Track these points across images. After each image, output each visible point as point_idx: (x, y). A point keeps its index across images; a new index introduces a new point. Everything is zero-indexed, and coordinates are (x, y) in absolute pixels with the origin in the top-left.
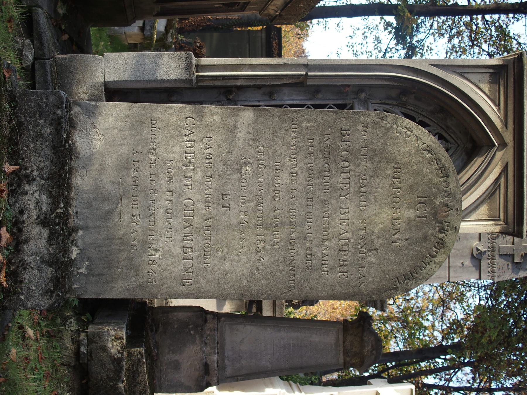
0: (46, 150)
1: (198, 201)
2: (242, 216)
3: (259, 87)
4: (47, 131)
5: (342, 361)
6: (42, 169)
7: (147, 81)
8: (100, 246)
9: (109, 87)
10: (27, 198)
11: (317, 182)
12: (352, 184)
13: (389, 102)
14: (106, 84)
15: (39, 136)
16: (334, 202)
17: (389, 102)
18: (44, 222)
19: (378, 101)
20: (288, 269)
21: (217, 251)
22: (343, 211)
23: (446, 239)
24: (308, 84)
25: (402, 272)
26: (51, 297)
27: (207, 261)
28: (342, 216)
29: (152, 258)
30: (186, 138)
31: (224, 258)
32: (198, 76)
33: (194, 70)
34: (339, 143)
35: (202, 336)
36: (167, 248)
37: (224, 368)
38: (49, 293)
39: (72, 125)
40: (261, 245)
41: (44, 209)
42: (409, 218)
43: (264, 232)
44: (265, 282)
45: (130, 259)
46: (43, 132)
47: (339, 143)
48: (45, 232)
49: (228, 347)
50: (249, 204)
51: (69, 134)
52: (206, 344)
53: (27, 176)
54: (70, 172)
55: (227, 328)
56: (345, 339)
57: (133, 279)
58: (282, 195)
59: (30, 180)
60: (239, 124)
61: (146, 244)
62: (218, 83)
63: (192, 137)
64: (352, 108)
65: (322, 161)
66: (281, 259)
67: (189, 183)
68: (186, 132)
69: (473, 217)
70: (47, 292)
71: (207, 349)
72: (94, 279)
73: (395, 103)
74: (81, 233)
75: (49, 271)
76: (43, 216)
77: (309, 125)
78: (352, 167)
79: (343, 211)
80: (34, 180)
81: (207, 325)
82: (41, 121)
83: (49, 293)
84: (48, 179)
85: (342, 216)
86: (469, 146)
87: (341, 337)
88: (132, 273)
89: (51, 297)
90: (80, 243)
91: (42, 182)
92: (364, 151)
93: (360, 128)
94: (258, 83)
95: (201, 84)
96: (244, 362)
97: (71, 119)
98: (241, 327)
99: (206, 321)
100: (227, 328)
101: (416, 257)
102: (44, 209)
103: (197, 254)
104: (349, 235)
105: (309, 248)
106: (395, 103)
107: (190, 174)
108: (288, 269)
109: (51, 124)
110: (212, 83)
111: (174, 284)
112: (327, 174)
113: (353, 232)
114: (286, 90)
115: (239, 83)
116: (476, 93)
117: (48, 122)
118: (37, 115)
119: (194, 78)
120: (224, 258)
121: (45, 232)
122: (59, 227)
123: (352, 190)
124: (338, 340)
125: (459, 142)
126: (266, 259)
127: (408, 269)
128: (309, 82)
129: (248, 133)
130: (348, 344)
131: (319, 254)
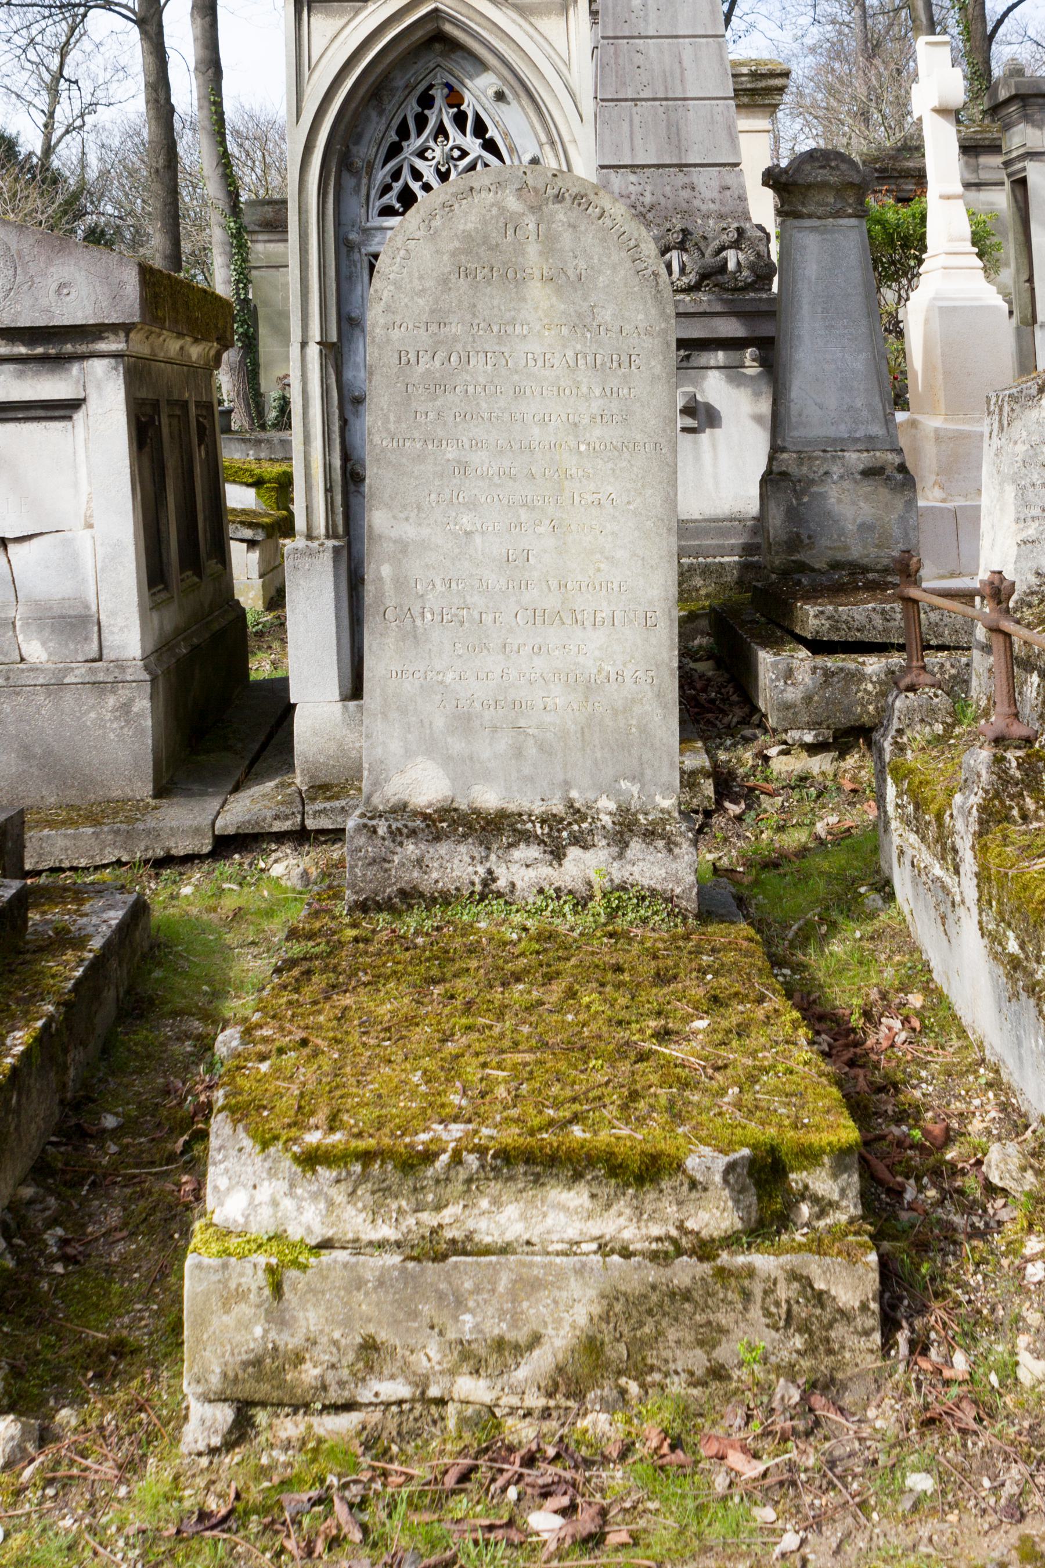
0: (443, 852)
1: (518, 602)
2: (541, 530)
3: (344, 422)
4: (411, 849)
5: (853, 221)
6: (473, 858)
7: (338, 626)
8: (596, 763)
9: (349, 692)
10: (519, 885)
11: (484, 405)
12: (487, 348)
13: (364, 190)
14: (344, 698)
15: (419, 862)
16: (516, 377)
17: (364, 190)
18: (557, 855)
19: (363, 211)
20: (626, 455)
21: (599, 570)
22: (531, 363)
23: (574, 191)
24: (335, 339)
25: (628, 264)
26: (676, 844)
27: (615, 586)
28: (540, 363)
29: (613, 676)
30: (419, 622)
31: (610, 559)
32: (328, 537)
33: (315, 544)
34: (421, 368)
35: (812, 482)
36: (597, 653)
37: (870, 438)
38: (671, 845)
39: (400, 809)
40: (590, 498)
41: (536, 855)
42: (541, 253)
43: (567, 494)
44: (649, 492)
45: (615, 712)
46: (414, 857)
47: (421, 368)
48: (573, 852)
49: (831, 432)
50: (523, 518)
51: (415, 814)
52: (826, 473)
53: (485, 884)
54: (476, 812)
55: (795, 434)
56: (810, 216)
57: (648, 708)
58: (506, 464)
59: (491, 877)
60: (394, 534)
61: (589, 688)
62: (338, 498)
63: (416, 611)
64: (376, 256)
65: (450, 397)
66: (610, 465)
67: (491, 617)
68: (408, 620)
69: (561, 46)
70: (670, 851)
71: (836, 470)
72: (648, 772)
73: (365, 181)
74: (574, 794)
75: (636, 846)
76: (549, 857)
77: (392, 418)
78: (459, 347)
79: (531, 363)
80: (490, 872)
81: (790, 470)
82: (396, 859)
83: (671, 845)
84: (488, 848)
85: (540, 363)
86: (438, 47)
87: (807, 223)
88: (637, 709)
89: (676, 844)
90: (591, 795)
91: (493, 857)
92: (433, 328)
93: (396, 334)
94: (336, 428)
95: (341, 530)
96: (859, 403)
97: (393, 811)
98: (794, 409)
99: (784, 475)
100: (795, 434)
101: (603, 240)
102: (536, 855)
103: (605, 604)
104: (570, 354)
105: (593, 418)
106: (365, 181)
107: (477, 617)
108: (626, 455)
109: (401, 844)
110: (339, 510)
111: (654, 641)
112: (471, 389)
113: (564, 346)
114: (349, 374)
115: (337, 462)
116: (344, 43)
117: (399, 849)
118: (387, 865)
119: (330, 543)
120: (610, 559)
121: (573, 852)
122: (560, 832)
123: (497, 348)
124: (813, 229)
125: (432, 65)
126: (610, 489)
127: (623, 254)
128: (334, 338)
129: (407, 519)
130: (820, 211)
131: (601, 401)
